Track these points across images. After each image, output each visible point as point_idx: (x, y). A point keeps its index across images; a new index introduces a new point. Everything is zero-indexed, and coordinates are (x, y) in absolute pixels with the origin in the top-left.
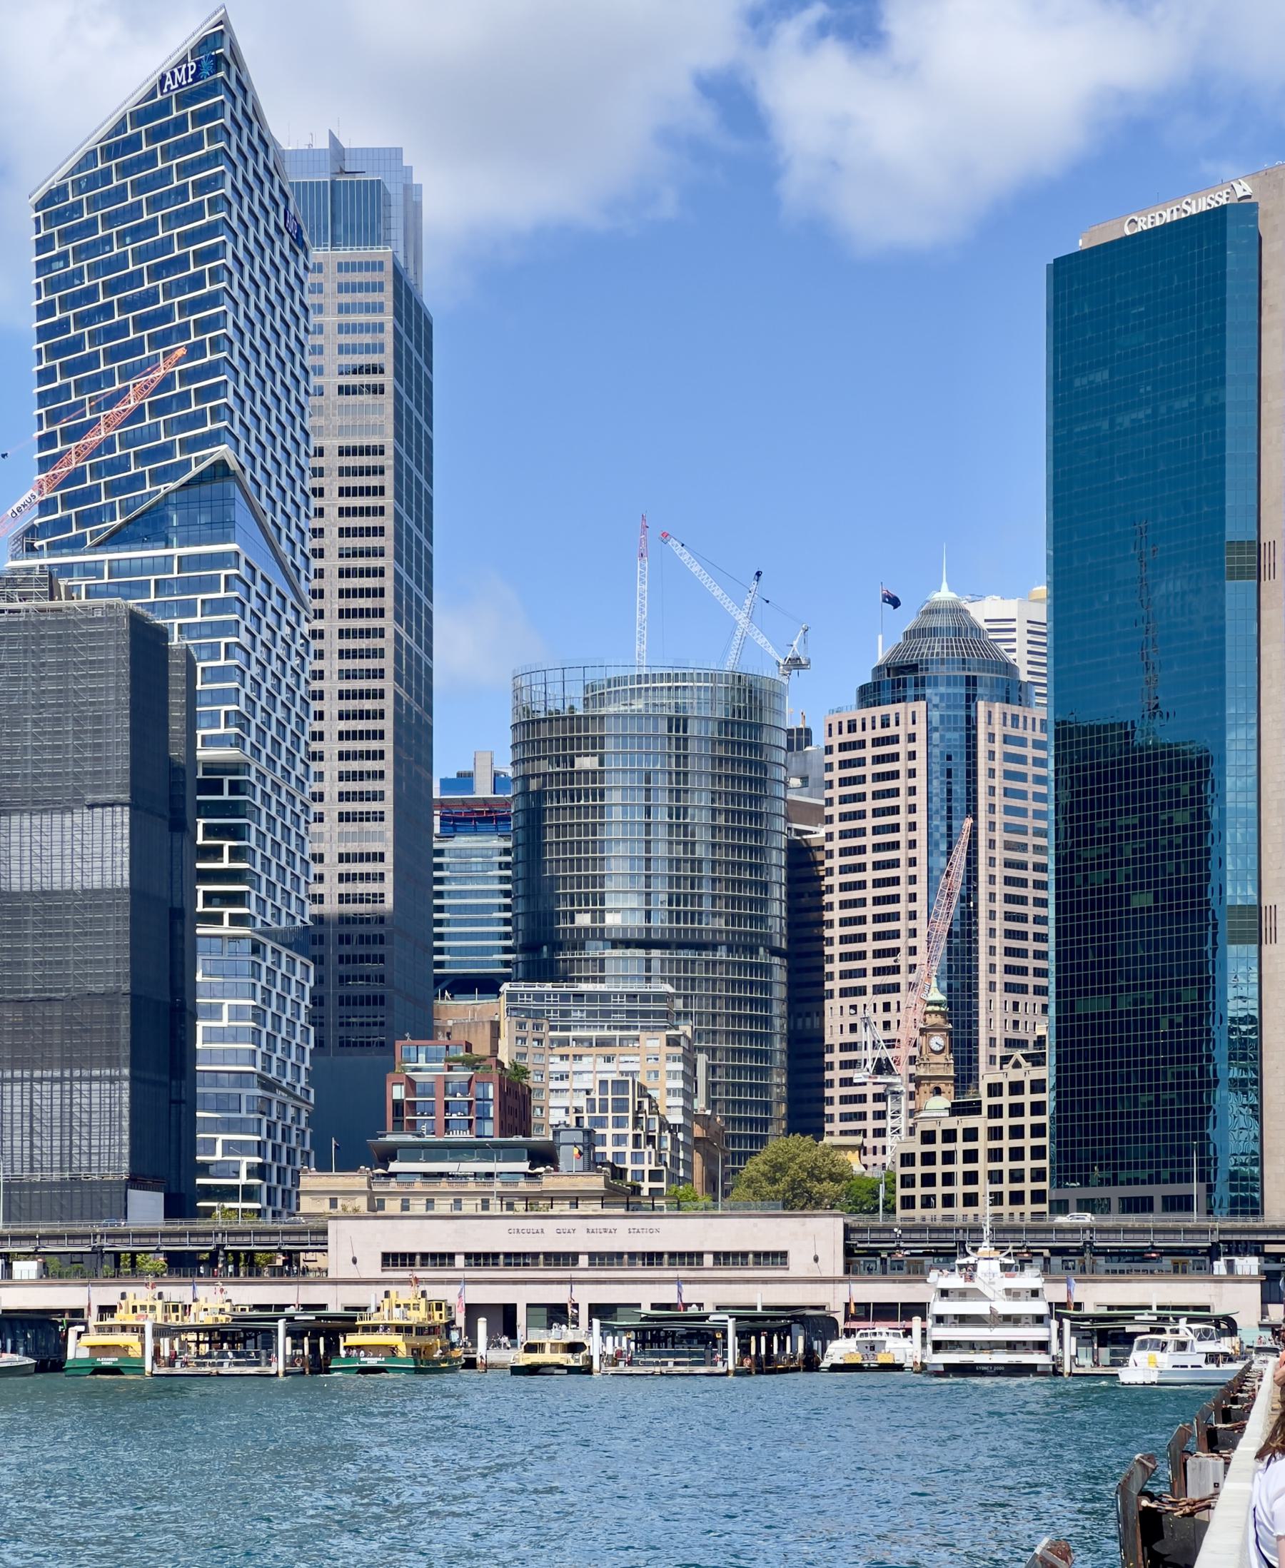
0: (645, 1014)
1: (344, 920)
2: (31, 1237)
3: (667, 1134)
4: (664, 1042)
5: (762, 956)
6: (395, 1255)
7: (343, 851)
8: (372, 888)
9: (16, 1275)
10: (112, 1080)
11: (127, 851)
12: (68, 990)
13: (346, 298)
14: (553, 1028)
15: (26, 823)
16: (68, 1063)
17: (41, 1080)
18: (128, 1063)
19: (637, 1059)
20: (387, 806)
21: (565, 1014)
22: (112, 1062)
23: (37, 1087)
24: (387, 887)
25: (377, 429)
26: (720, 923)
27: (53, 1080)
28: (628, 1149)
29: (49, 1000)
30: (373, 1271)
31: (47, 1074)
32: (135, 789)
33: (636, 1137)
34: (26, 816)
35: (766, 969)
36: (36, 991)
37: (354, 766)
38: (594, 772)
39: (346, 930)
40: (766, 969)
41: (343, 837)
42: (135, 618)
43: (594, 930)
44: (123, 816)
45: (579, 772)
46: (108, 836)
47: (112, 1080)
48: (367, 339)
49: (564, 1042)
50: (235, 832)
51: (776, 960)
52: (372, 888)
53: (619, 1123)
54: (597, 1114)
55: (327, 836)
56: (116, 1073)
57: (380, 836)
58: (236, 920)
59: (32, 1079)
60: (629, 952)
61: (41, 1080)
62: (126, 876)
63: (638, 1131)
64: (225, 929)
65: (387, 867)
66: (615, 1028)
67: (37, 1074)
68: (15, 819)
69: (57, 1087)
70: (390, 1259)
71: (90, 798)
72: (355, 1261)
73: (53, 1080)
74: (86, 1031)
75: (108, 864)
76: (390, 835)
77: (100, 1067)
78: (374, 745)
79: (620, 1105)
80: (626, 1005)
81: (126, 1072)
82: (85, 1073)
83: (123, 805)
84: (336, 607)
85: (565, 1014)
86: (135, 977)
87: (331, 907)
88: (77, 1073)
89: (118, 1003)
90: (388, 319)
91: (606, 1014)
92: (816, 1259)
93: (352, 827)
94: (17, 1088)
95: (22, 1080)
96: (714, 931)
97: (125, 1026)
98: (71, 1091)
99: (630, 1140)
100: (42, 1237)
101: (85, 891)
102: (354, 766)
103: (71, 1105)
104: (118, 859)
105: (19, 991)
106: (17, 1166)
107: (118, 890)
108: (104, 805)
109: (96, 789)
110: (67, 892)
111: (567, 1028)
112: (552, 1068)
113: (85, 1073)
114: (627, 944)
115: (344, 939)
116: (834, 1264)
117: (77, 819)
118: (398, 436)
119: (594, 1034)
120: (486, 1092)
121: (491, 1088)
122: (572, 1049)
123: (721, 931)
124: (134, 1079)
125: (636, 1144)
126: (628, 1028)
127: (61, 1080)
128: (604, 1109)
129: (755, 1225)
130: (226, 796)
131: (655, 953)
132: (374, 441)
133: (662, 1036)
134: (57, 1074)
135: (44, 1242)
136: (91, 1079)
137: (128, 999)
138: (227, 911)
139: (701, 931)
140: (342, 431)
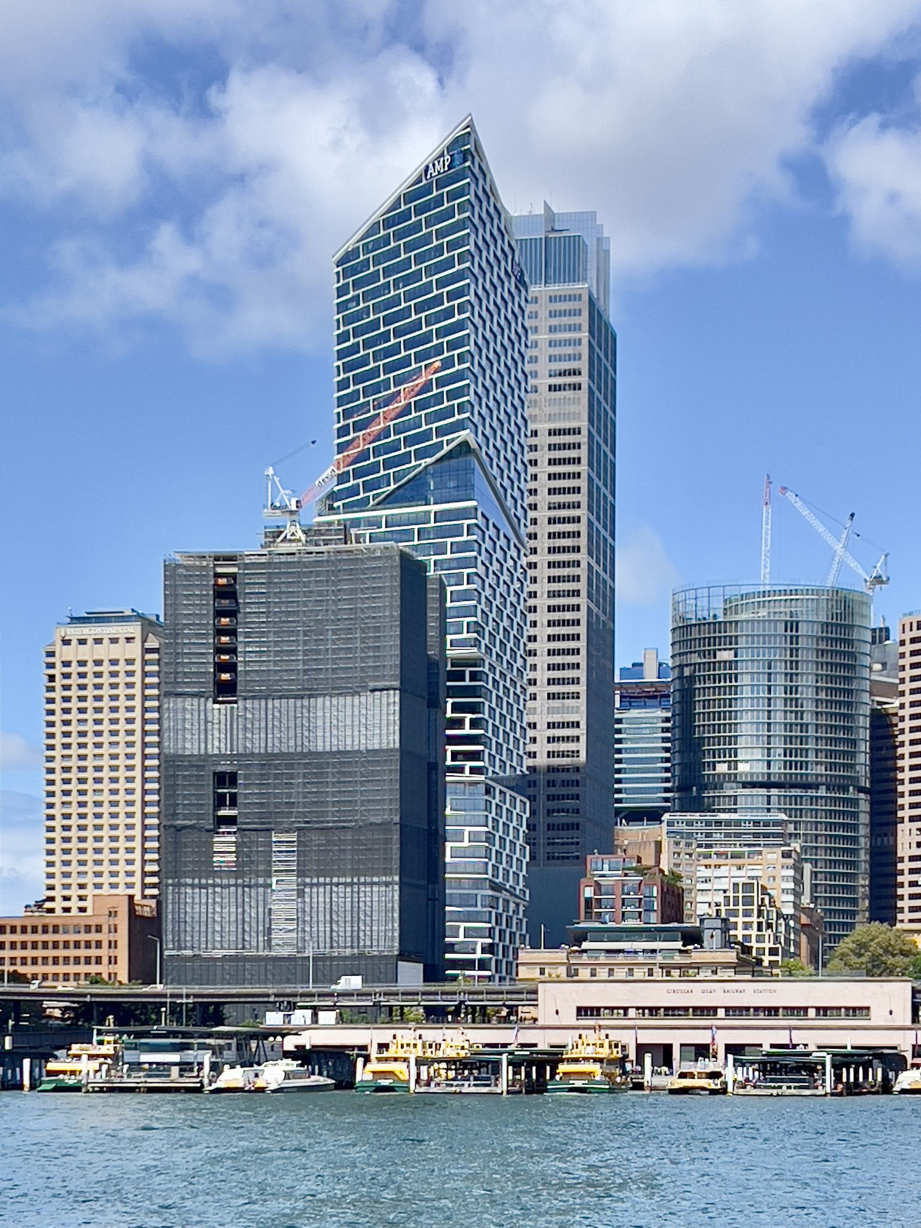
0: (766, 835)
1: (551, 769)
3: (781, 921)
5: (852, 793)
8: (571, 746)
10: (387, 884)
11: (398, 722)
12: (356, 821)
13: (555, 321)
14: (700, 846)
15: (328, 703)
16: (356, 872)
17: (337, 885)
19: (760, 867)
20: (582, 689)
23: (335, 889)
24: (582, 746)
25: (577, 416)
26: (821, 770)
27: (346, 884)
28: (754, 932)
29: (344, 827)
30: (572, 1020)
31: (342, 880)
33: (760, 924)
34: (327, 698)
36: (334, 822)
37: (559, 660)
38: (730, 662)
39: (551, 776)
40: (854, 803)
41: (550, 711)
42: (403, 556)
43: (730, 775)
44: (394, 697)
45: (720, 662)
46: (384, 712)
47: (387, 884)
48: (569, 350)
50: (473, 708)
51: (862, 796)
52: (571, 746)
53: (747, 914)
54: (731, 907)
55: (539, 710)
56: (389, 879)
57: (577, 710)
58: (473, 770)
59: (331, 884)
60: (755, 791)
61: (337, 885)
62: (397, 740)
63: (761, 919)
64: (467, 776)
65: (582, 732)
67: (335, 880)
68: (320, 700)
69: (349, 889)
70: (582, 1011)
71: (372, 685)
72: (557, 1012)
73: (346, 884)
75: (384, 732)
76: (584, 709)
77: (378, 875)
78: (572, 645)
80: (753, 829)
81: (397, 878)
82: (368, 879)
83: (395, 689)
84: (546, 546)
85: (708, 835)
87: (541, 761)
88: (362, 879)
92: (891, 1013)
93: (556, 703)
94: (321, 890)
95: (325, 884)
96: (817, 775)
97: (396, 846)
98: (358, 893)
99: (755, 926)
101: (368, 751)
102: (559, 660)
103: (359, 902)
105: (322, 822)
106: (322, 945)
107: (391, 750)
108: (381, 690)
109: (376, 678)
110: (356, 752)
111: (710, 846)
112: (699, 874)
113: (368, 879)
114: (754, 785)
115: (551, 784)
116: (589, 974)
117: (363, 699)
118: (591, 421)
121: (655, 888)
122: (714, 860)
123: (822, 775)
124: (402, 884)
125: (760, 928)
126: (754, 845)
127: (352, 884)
128: (736, 904)
130: (467, 683)
131: (774, 791)
132: (573, 424)
134: (349, 880)
135: (340, 998)
136: (372, 884)
139: (807, 775)
140: (550, 418)
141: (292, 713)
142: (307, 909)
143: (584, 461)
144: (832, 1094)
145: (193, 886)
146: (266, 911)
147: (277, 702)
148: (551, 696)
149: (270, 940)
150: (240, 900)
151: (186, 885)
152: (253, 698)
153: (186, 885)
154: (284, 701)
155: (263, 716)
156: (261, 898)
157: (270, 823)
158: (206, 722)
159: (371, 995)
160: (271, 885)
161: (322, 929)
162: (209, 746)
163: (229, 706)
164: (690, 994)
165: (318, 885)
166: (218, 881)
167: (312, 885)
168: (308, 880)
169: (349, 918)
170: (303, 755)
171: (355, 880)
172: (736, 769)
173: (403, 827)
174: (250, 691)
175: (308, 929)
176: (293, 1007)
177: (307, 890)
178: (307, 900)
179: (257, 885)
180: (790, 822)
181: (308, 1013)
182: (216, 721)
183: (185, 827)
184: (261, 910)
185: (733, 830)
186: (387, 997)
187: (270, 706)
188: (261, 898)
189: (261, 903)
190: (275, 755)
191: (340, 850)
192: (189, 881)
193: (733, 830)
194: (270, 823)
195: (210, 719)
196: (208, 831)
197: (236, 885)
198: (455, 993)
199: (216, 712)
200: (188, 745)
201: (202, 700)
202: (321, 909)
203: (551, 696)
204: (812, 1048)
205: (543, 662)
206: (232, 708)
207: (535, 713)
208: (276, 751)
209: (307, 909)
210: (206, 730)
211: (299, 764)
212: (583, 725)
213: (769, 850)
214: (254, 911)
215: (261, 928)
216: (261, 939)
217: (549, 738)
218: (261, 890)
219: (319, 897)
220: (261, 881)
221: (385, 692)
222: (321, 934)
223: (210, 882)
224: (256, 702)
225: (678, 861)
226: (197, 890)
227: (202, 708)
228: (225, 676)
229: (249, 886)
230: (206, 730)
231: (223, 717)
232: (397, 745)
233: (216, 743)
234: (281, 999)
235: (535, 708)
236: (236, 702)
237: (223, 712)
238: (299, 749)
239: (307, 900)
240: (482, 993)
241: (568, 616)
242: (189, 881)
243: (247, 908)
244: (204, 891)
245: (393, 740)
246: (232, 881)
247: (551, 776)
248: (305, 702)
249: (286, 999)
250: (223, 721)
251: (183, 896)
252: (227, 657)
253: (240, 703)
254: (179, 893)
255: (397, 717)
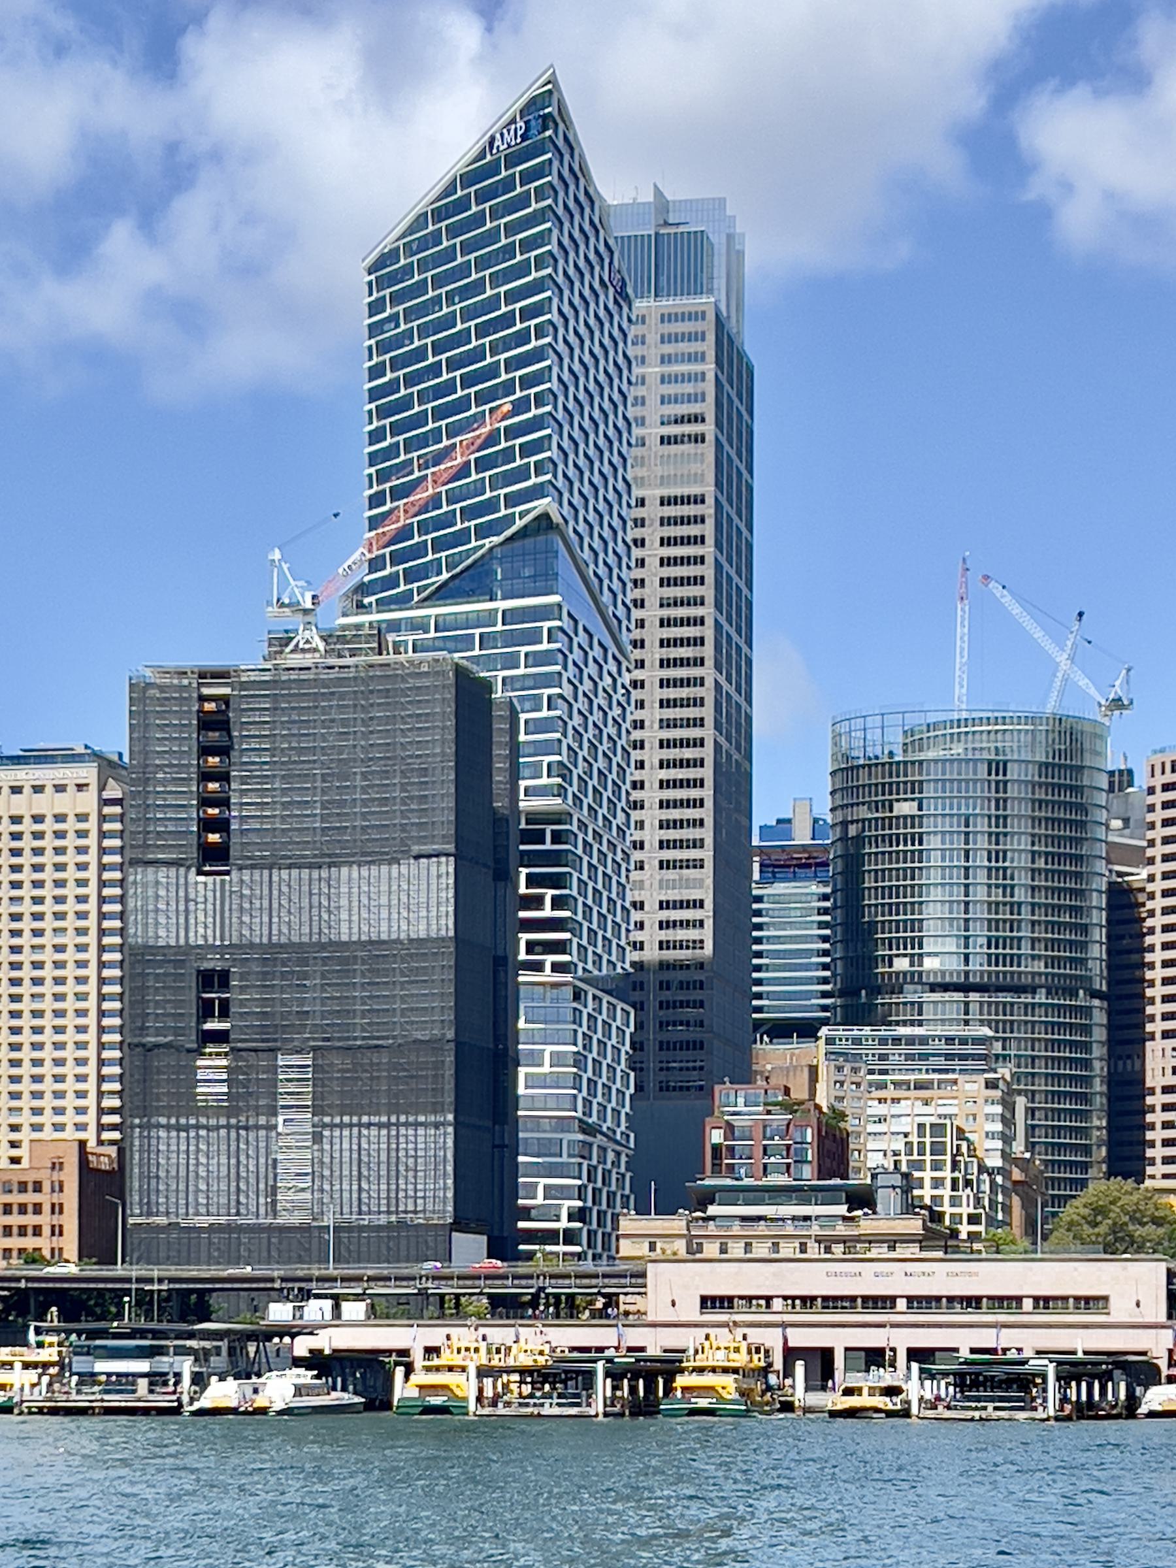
1: (664, 966)
2: (359, 1279)
3: (985, 1177)
4: (983, 1085)
5: (1082, 999)
6: (713, 1299)
7: (664, 898)
8: (692, 934)
9: (346, 1316)
11: (452, 901)
12: (394, 1037)
13: (668, 349)
14: (871, 1072)
15: (355, 874)
17: (369, 1125)
18: (452, 1108)
19: (955, 1102)
21: (884, 1057)
22: (436, 1109)
23: (365, 1132)
24: (707, 934)
25: (698, 479)
26: (1040, 967)
27: (380, 1126)
29: (377, 1046)
31: (375, 1119)
32: (459, 840)
33: (954, 1181)
34: (355, 867)
35: (1086, 1011)
38: (913, 817)
39: (667, 976)
40: (1086, 1011)
41: (662, 884)
43: (913, 973)
44: (448, 866)
45: (898, 818)
46: (434, 887)
48: (688, 388)
49: (882, 1086)
50: (556, 881)
51: (1096, 1002)
52: (692, 934)
53: (937, 1166)
54: (915, 1157)
55: (647, 884)
57: (700, 883)
58: (556, 967)
59: (360, 1125)
60: (947, 996)
61: (369, 1125)
62: (451, 925)
63: (957, 1174)
64: (547, 976)
66: (934, 1071)
67: (365, 1119)
68: (345, 870)
70: (709, 1302)
71: (416, 849)
72: (673, 1304)
73: (380, 1126)
74: (412, 1077)
75: (434, 913)
76: (709, 882)
79: (938, 1149)
83: (447, 855)
84: (658, 656)
86: (459, 1024)
87: (651, 954)
88: (403, 1119)
89: (442, 1049)
90: (710, 368)
91: (924, 1057)
92: (1138, 1305)
93: (672, 874)
94: (346, 1132)
95: (351, 1125)
99: (948, 1183)
100: (370, 1279)
103: (397, 1150)
104: (443, 909)
105: (348, 1039)
106: (346, 1209)
107: (443, 939)
108: (429, 856)
109: (421, 840)
112: (869, 1111)
113: (411, 1119)
114: (946, 988)
115: (664, 985)
117: (404, 869)
118: (718, 484)
119: (912, 1077)
120: (804, 1135)
121: (809, 1131)
122: (891, 1092)
123: (1040, 974)
124: (457, 1124)
125: (954, 1188)
126: (947, 1071)
128: (921, 1152)
129: (1076, 1269)
131: (974, 996)
133: (981, 1079)
134: (384, 1119)
135: (372, 1284)
136: (417, 1124)
137: (452, 1045)
138: (550, 959)
140: (664, 481)
141: (305, 888)
142: (327, 1160)
143: (710, 540)
144: (1057, 1419)
145: (168, 1127)
146: (270, 1162)
147: (284, 874)
148: (663, 865)
149: (274, 1203)
150: (233, 1148)
151: (159, 1126)
152: (253, 867)
153: (159, 1126)
154: (295, 872)
155: (266, 892)
156: (262, 1144)
157: (275, 1040)
158: (187, 900)
159: (414, 1279)
160: (275, 1127)
161: (346, 1186)
162: (191, 934)
163: (218, 878)
164: (859, 1278)
165: (341, 1126)
166: (203, 1120)
167: (332, 1126)
168: (327, 1119)
169: (383, 1173)
170: (322, 946)
171: (393, 1119)
172: (921, 965)
173: (460, 1045)
174: (249, 858)
175: (327, 1187)
176: (306, 1295)
177: (326, 1133)
178: (327, 1147)
179: (258, 1127)
180: (997, 1039)
181: (328, 1304)
182: (201, 899)
183: (157, 1046)
184: (262, 1160)
185: (917, 1049)
186: (436, 1282)
187: (275, 878)
188: (262, 1144)
189: (262, 1151)
190: (281, 946)
191: (372, 1078)
192: (163, 1120)
193: (917, 1049)
194: (275, 1040)
195: (192, 896)
196: (189, 1051)
197: (228, 1127)
198: (531, 1277)
199: (201, 887)
200: (162, 933)
201: (182, 870)
202: (346, 1159)
203: (663, 865)
204: (1028, 1353)
205: (653, 818)
206: (223, 881)
207: (642, 889)
208: (284, 940)
209: (327, 1160)
210: (187, 911)
211: (315, 958)
212: (709, 904)
213: (967, 1077)
214: (252, 1162)
215: (262, 1186)
216: (262, 1200)
217: (661, 923)
218: (262, 1133)
219: (342, 1142)
220: (262, 1120)
221: (434, 859)
222: (346, 1195)
223: (193, 1121)
224: (257, 873)
225: (842, 1094)
226: (174, 1134)
227: (182, 881)
228: (214, 838)
229: (246, 1128)
230: (187, 911)
231: (210, 894)
232: (451, 933)
233: (201, 931)
234: (290, 1285)
235: (642, 881)
236: (227, 873)
237: (210, 887)
238: (315, 938)
239: (327, 1147)
240: (568, 1276)
241: (688, 753)
242: (163, 1120)
243: (243, 1158)
244: (183, 1134)
245: (446, 926)
246: (223, 1121)
247: (667, 976)
248: (324, 873)
249: (297, 1285)
250: (211, 900)
251: (154, 1142)
252: (216, 811)
253: (235, 874)
254: (149, 1137)
255: (451, 893)
